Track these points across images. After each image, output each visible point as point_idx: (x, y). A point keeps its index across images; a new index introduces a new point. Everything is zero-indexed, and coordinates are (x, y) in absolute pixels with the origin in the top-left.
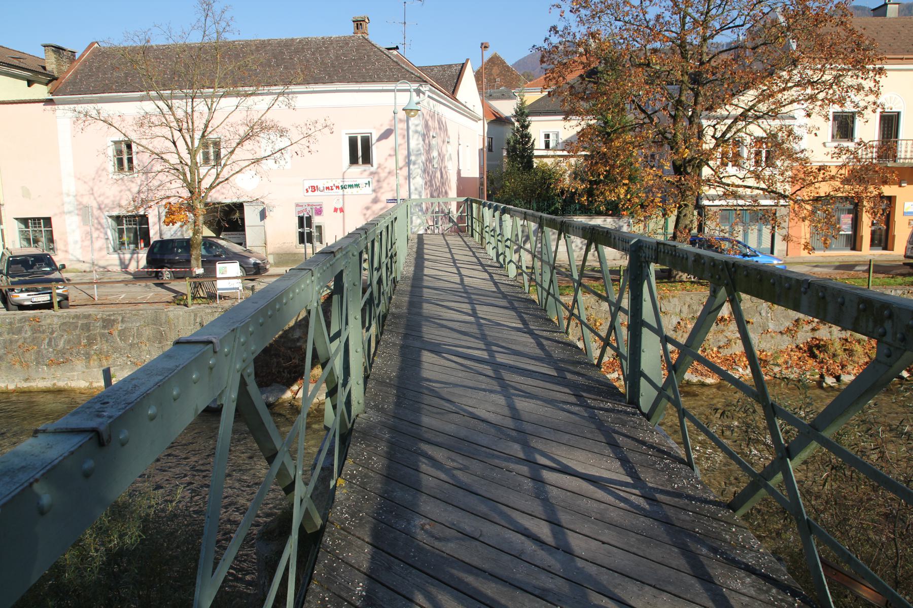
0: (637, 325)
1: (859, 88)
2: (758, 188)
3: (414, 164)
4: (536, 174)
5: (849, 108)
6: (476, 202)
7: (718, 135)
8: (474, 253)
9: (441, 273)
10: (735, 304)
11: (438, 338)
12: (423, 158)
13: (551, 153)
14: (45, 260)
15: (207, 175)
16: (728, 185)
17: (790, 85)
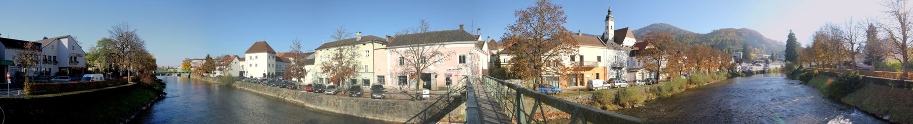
0: (519, 110)
14: (381, 86)
15: (422, 66)
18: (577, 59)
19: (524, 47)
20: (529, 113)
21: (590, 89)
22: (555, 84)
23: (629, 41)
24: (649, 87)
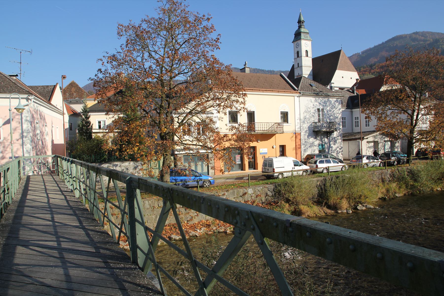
1: (237, 101)
2: (199, 145)
3: (26, 137)
4: (94, 142)
5: (234, 109)
6: (60, 157)
7: (180, 121)
8: (58, 185)
9: (37, 197)
10: (174, 208)
11: (29, 237)
12: (31, 134)
13: (101, 131)
16: (186, 144)
17: (209, 99)
18: (243, 119)
19: (139, 97)
20: (152, 224)
21: (268, 176)
22: (201, 168)
23: (345, 78)
24: (389, 170)
